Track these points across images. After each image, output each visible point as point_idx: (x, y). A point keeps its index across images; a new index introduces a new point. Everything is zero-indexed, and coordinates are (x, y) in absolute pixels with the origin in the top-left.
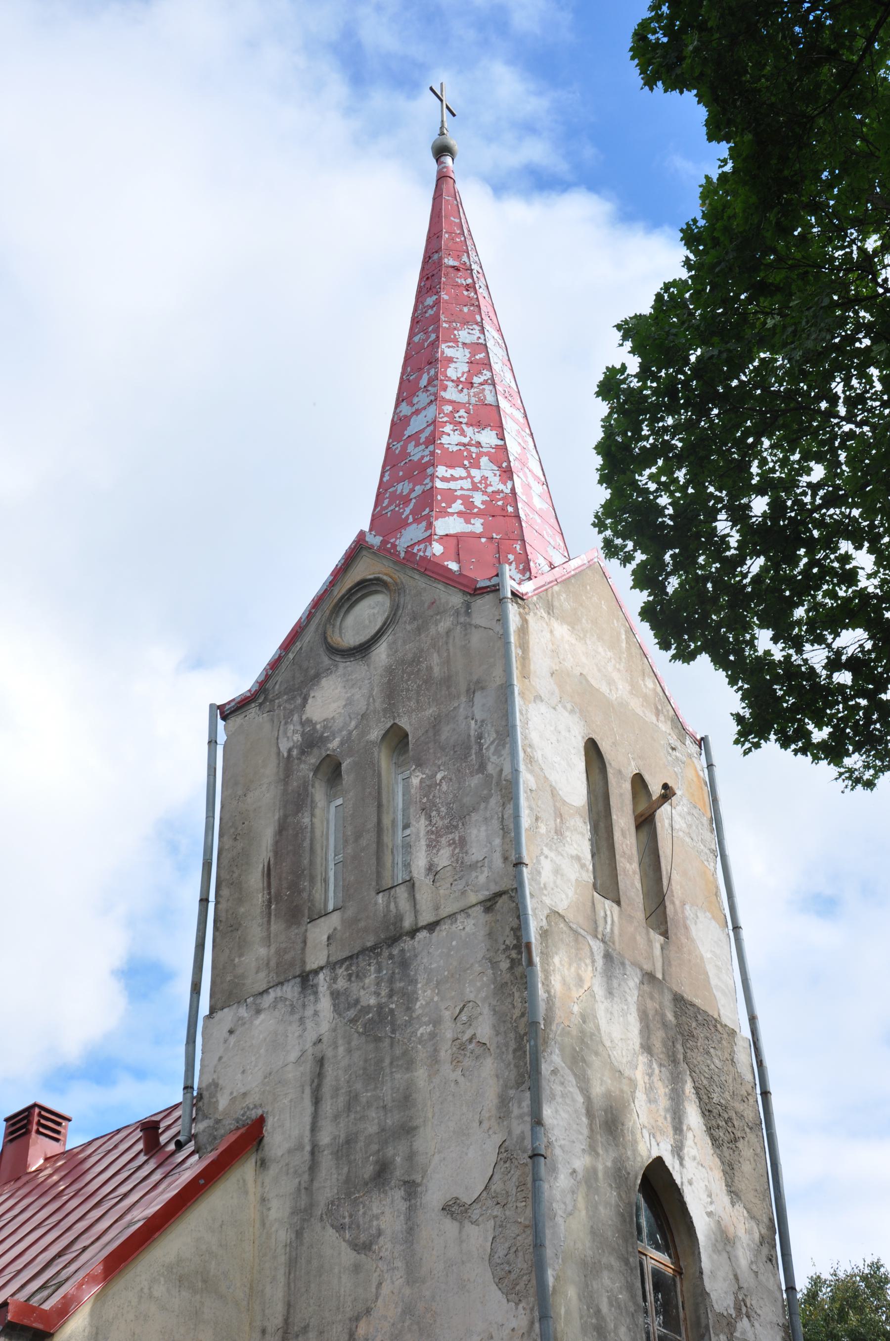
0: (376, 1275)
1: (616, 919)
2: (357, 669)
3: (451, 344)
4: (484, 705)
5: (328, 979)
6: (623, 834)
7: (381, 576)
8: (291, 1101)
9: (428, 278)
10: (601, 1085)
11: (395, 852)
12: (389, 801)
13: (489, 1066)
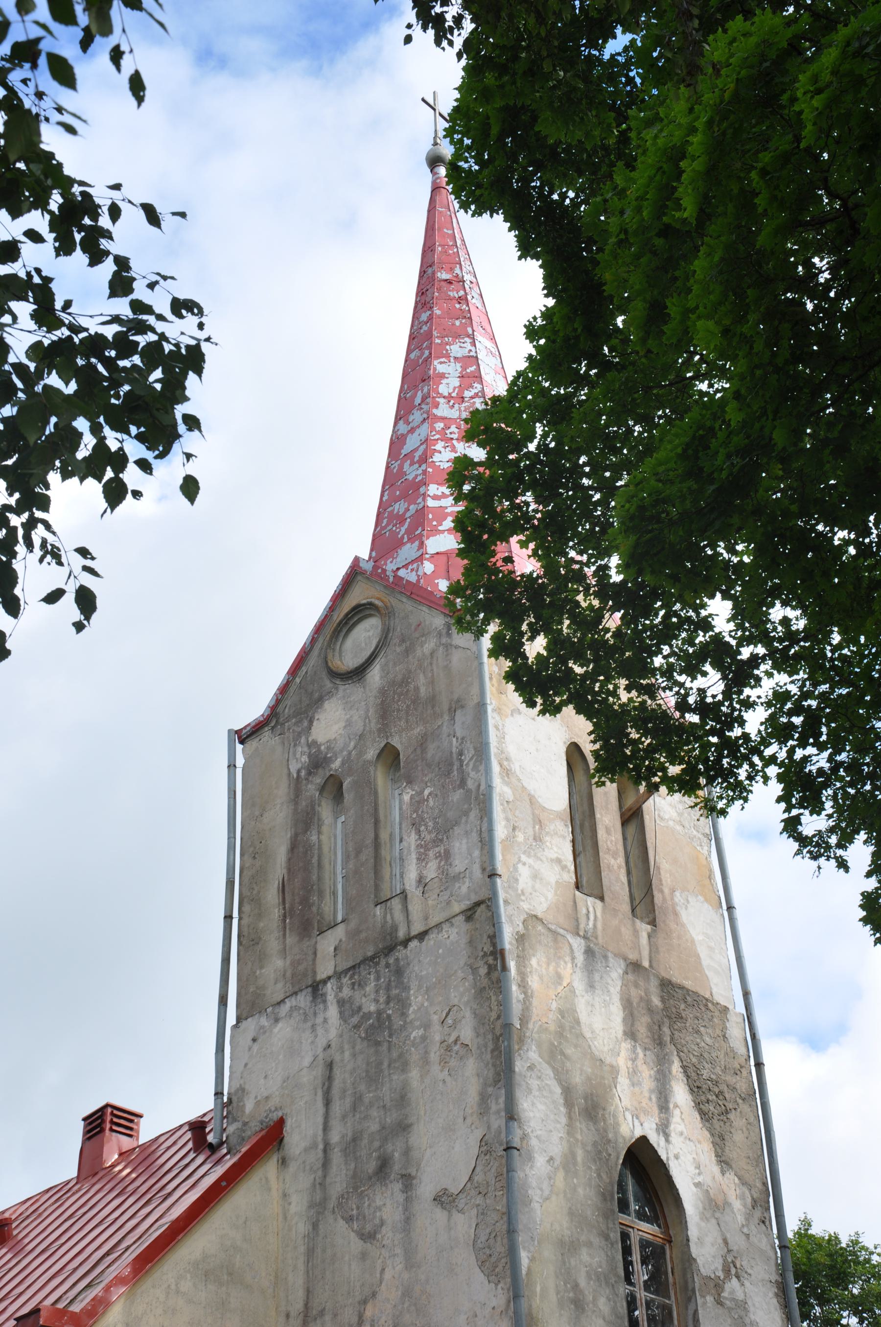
0: (380, 1261)
1: (599, 914)
2: (354, 691)
3: (443, 360)
4: (463, 723)
5: (334, 988)
6: (608, 831)
7: (373, 600)
8: (306, 1102)
9: (423, 293)
10: (581, 1074)
11: (393, 865)
12: (386, 817)
13: (471, 1066)
